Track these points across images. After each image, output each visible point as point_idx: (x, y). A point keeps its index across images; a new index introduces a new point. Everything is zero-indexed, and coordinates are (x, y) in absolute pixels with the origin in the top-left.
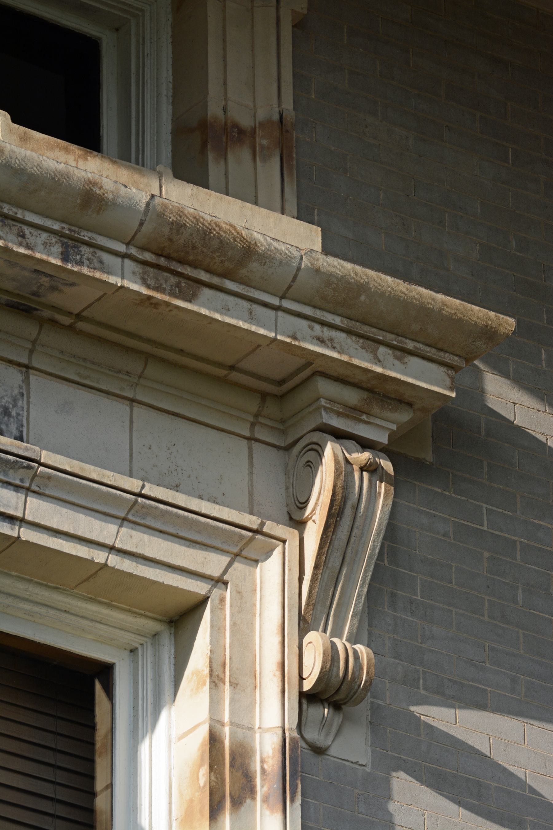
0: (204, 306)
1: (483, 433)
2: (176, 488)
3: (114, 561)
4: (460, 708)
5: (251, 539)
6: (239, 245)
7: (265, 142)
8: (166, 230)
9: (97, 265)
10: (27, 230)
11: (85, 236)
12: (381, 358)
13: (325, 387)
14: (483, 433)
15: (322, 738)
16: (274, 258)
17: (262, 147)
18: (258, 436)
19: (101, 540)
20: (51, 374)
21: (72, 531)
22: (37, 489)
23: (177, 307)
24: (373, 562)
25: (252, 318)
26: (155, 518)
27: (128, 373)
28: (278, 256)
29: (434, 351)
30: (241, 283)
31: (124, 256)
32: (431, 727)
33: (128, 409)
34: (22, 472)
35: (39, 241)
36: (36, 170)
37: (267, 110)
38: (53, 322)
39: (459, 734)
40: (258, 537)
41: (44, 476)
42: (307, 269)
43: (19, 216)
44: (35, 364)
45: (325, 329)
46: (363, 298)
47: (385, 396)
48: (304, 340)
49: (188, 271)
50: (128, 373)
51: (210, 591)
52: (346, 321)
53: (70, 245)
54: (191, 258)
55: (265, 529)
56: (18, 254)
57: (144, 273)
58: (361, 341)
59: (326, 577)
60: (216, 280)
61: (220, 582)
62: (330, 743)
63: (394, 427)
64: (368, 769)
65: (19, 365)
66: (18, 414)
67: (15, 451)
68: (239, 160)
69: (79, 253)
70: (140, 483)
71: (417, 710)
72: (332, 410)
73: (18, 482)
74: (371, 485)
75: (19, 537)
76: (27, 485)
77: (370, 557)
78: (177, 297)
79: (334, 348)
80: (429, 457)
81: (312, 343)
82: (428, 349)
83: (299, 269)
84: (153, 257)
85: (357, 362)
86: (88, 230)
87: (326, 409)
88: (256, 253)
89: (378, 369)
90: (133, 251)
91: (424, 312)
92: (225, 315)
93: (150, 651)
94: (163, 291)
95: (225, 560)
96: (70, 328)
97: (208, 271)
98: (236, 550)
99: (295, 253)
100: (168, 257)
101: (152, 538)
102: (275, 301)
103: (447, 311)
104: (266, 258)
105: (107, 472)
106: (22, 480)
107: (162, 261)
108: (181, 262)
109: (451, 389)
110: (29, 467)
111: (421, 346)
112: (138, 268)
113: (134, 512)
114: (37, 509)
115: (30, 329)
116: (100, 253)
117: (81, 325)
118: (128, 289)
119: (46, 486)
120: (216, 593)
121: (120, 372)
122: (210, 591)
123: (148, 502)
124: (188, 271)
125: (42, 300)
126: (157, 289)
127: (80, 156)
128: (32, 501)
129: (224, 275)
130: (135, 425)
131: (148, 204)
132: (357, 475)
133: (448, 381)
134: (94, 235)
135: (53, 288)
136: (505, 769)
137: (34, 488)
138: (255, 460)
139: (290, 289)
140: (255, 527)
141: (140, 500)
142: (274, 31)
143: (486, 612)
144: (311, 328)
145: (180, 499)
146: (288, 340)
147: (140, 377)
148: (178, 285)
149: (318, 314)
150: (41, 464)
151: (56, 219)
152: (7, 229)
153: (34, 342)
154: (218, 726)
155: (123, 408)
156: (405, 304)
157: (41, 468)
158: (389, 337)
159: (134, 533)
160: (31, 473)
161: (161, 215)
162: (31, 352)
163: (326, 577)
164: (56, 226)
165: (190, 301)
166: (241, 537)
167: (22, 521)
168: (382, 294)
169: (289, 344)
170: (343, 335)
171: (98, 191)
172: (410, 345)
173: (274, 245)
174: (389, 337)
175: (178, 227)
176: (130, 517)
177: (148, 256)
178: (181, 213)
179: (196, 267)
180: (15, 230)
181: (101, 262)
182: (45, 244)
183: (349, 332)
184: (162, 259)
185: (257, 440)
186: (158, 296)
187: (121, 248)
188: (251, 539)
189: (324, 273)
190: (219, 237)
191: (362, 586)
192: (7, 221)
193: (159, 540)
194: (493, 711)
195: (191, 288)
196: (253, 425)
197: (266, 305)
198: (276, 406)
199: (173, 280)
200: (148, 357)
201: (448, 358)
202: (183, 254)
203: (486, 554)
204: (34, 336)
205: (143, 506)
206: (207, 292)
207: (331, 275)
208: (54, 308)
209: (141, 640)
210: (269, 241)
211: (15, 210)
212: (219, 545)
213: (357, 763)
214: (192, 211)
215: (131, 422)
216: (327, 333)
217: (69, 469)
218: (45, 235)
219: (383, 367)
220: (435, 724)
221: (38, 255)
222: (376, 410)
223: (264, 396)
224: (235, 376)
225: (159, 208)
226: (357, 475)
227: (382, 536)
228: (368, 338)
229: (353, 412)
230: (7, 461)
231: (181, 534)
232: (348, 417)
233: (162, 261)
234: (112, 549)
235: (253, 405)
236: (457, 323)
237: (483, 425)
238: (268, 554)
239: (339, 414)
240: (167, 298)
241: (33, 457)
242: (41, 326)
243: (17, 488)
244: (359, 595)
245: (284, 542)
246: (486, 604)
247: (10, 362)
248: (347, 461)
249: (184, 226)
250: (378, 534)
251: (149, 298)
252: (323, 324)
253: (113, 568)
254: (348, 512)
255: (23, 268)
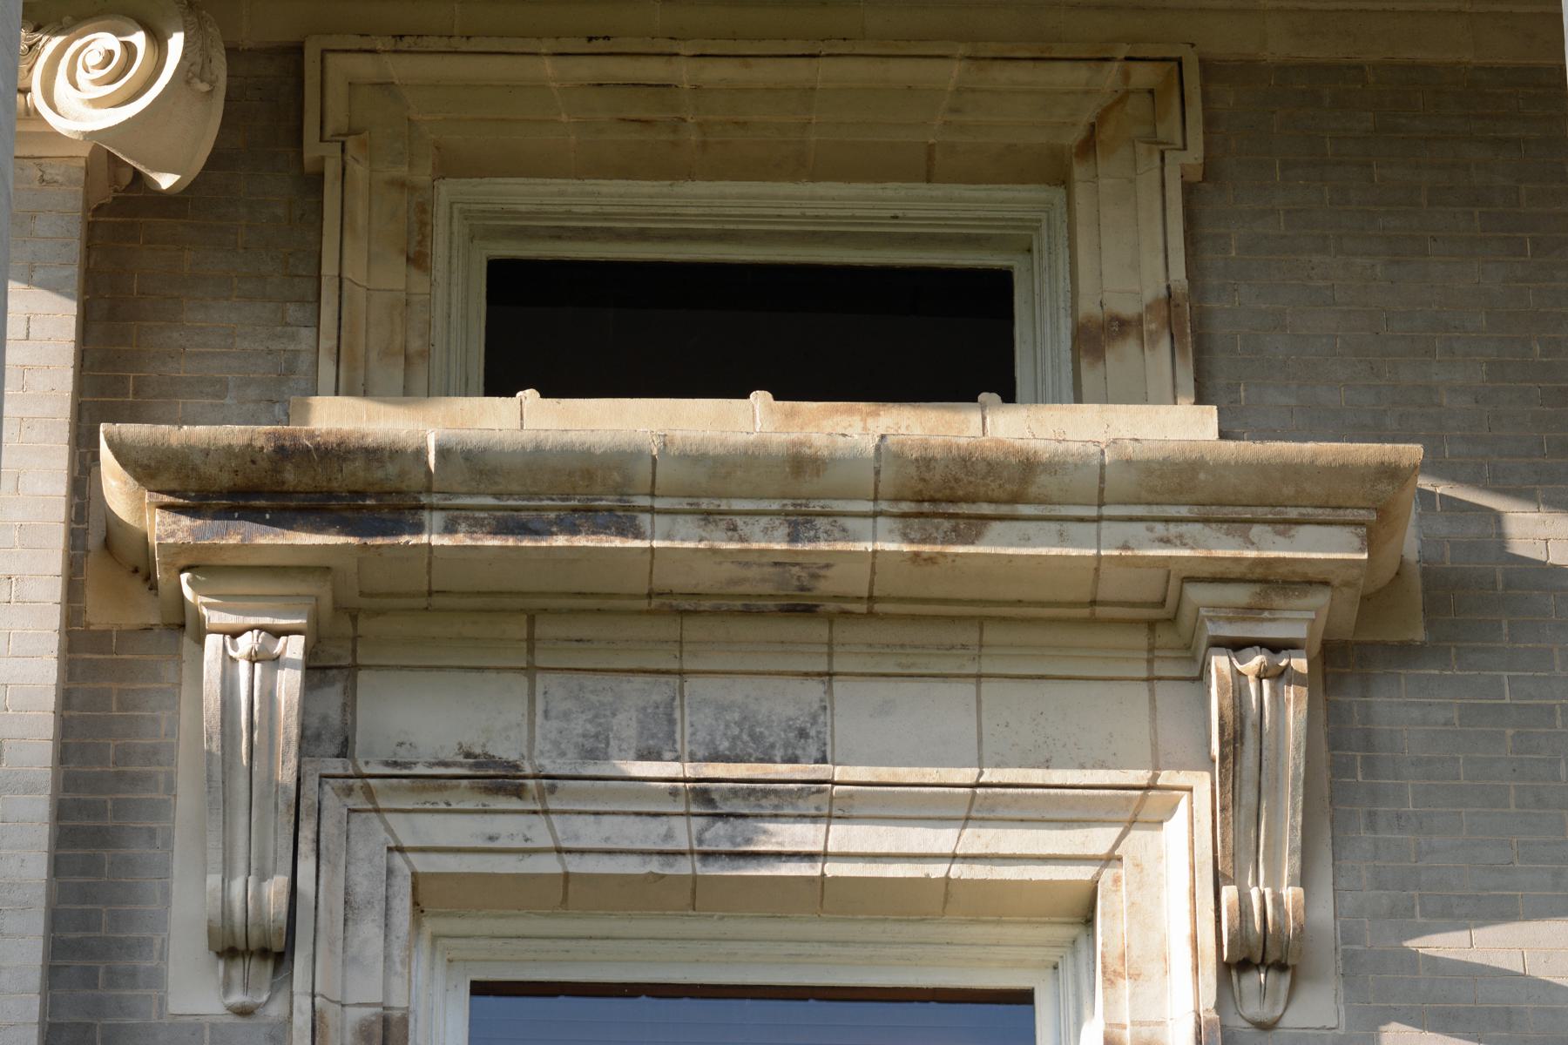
0: (993, 544)
1: (1500, 587)
2: (1047, 764)
3: (959, 871)
4: (1477, 926)
5: (1143, 799)
6: (1013, 460)
7: (1153, 326)
8: (912, 470)
9: (837, 534)
10: (739, 521)
11: (816, 506)
12: (1255, 540)
13: (1198, 595)
14: (1500, 587)
15: (1266, 1008)
16: (1065, 463)
17: (1151, 333)
18: (1157, 673)
19: (936, 850)
20: (863, 675)
21: (893, 850)
22: (840, 813)
23: (957, 555)
24: (1301, 783)
25: (1063, 540)
26: (1007, 806)
27: (964, 646)
28: (1070, 459)
29: (1328, 511)
30: (1041, 503)
31: (875, 515)
32: (1434, 959)
33: (973, 688)
34: (814, 800)
35: (757, 529)
36: (721, 451)
37: (1153, 289)
38: (846, 614)
39: (1475, 958)
40: (1152, 793)
41: (841, 796)
42: (1114, 463)
43: (724, 507)
44: (837, 668)
45: (1171, 526)
46: (1202, 476)
47: (1285, 582)
48: (1140, 547)
49: (965, 508)
50: (964, 646)
51: (1099, 874)
52: (1195, 509)
53: (799, 522)
54: (960, 493)
55: (1159, 782)
56: (731, 552)
57: (906, 527)
58: (1225, 526)
59: (1242, 818)
60: (1004, 509)
61: (1111, 859)
62: (1278, 1013)
63: (1312, 615)
64: (1341, 1031)
65: (819, 674)
66: (819, 732)
67: (798, 777)
68: (1123, 356)
69: (813, 528)
70: (977, 770)
71: (1411, 944)
72: (1220, 618)
73: (813, 812)
74: (1275, 693)
75: (823, 875)
76: (826, 811)
77: (1295, 778)
78: (953, 543)
79: (1184, 545)
80: (1419, 635)
81: (1152, 548)
82: (1320, 511)
83: (1102, 466)
84: (913, 505)
85: (1220, 553)
86: (818, 498)
87: (1211, 619)
88: (1039, 464)
89: (1252, 554)
90: (884, 506)
91: (1291, 471)
92: (1024, 546)
93: (1069, 961)
94: (934, 541)
95: (1115, 832)
96: (871, 614)
97: (991, 501)
98: (1128, 816)
99: (1092, 449)
100: (932, 500)
101: (1009, 831)
102: (1092, 512)
103: (1321, 461)
104: (1054, 466)
105: (928, 770)
106: (817, 808)
107: (926, 507)
108: (952, 501)
109: (1361, 550)
110: (819, 791)
111: (1310, 510)
112: (896, 524)
113: (977, 807)
114: (842, 836)
115: (819, 631)
116: (841, 521)
117: (878, 607)
118: (883, 552)
119: (851, 806)
120: (1108, 874)
121: (953, 647)
122: (1099, 874)
123: (989, 790)
124: (965, 508)
125: (814, 593)
126: (923, 541)
127: (868, 414)
128: (837, 829)
129: (1015, 499)
130: (984, 706)
131: (878, 448)
132: (1253, 687)
133: (1357, 542)
134: (827, 502)
135: (814, 576)
136: (1549, 983)
137: (836, 812)
138: (1158, 704)
139: (1171, 487)
140: (1144, 783)
141: (978, 791)
142: (1158, 197)
143: (1512, 802)
144: (1151, 530)
145: (1056, 776)
146: (1116, 553)
147: (981, 646)
148: (955, 529)
149: (1156, 511)
150: (835, 783)
151: (775, 498)
152: (711, 527)
153: (830, 644)
154: (1116, 1031)
155: (968, 688)
156: (1262, 468)
157: (837, 788)
158: (1260, 512)
159: (982, 831)
160: (826, 797)
161: (898, 456)
162: (830, 655)
163: (1242, 818)
164: (775, 506)
165: (973, 543)
166: (1129, 799)
167: (825, 856)
168: (1226, 465)
169: (1120, 557)
170: (1199, 526)
171: (808, 451)
172: (1293, 513)
173: (1061, 447)
174: (1260, 512)
175: (926, 462)
176: (974, 814)
177: (906, 507)
178: (925, 446)
179: (974, 502)
180: (723, 525)
181: (844, 530)
182: (765, 530)
183: (1206, 521)
184: (926, 504)
185: (1160, 679)
186: (926, 548)
187: (868, 507)
188: (1143, 799)
189: (1138, 462)
190: (984, 459)
191: (1293, 816)
192: (711, 518)
193: (1020, 831)
194: (1527, 919)
195: (973, 527)
196: (1150, 662)
197: (1081, 520)
198: (1157, 629)
199: (947, 524)
200: (981, 622)
201: (1349, 515)
202: (948, 492)
203: (1510, 732)
204: (825, 637)
205: (986, 797)
206: (997, 527)
207: (1148, 461)
208: (836, 598)
209: (1059, 952)
210: (1053, 445)
211: (717, 502)
212: (1103, 817)
213: (1323, 1028)
214: (940, 439)
215: (979, 702)
216: (1174, 529)
217: (875, 780)
218: (764, 521)
219: (1258, 549)
220: (1440, 954)
221: (755, 546)
222: (1278, 601)
223: (1151, 625)
224: (1100, 611)
225: (894, 449)
226: (1253, 687)
227: (1303, 750)
228: (1234, 521)
229: (1249, 612)
230: (790, 791)
231: (1048, 816)
232: (1244, 620)
233: (926, 507)
234: (954, 857)
235: (1140, 639)
236: (1342, 471)
237: (1500, 577)
238: (1173, 810)
239: (1230, 620)
240: (938, 548)
241: (823, 777)
242: (831, 623)
243: (815, 819)
244: (1293, 828)
245: (1190, 790)
246: (1513, 791)
247: (806, 674)
248: (1239, 673)
249: (933, 459)
250: (1297, 749)
251: (917, 554)
252: (1167, 520)
253: (958, 880)
254: (1250, 735)
255: (761, 565)
